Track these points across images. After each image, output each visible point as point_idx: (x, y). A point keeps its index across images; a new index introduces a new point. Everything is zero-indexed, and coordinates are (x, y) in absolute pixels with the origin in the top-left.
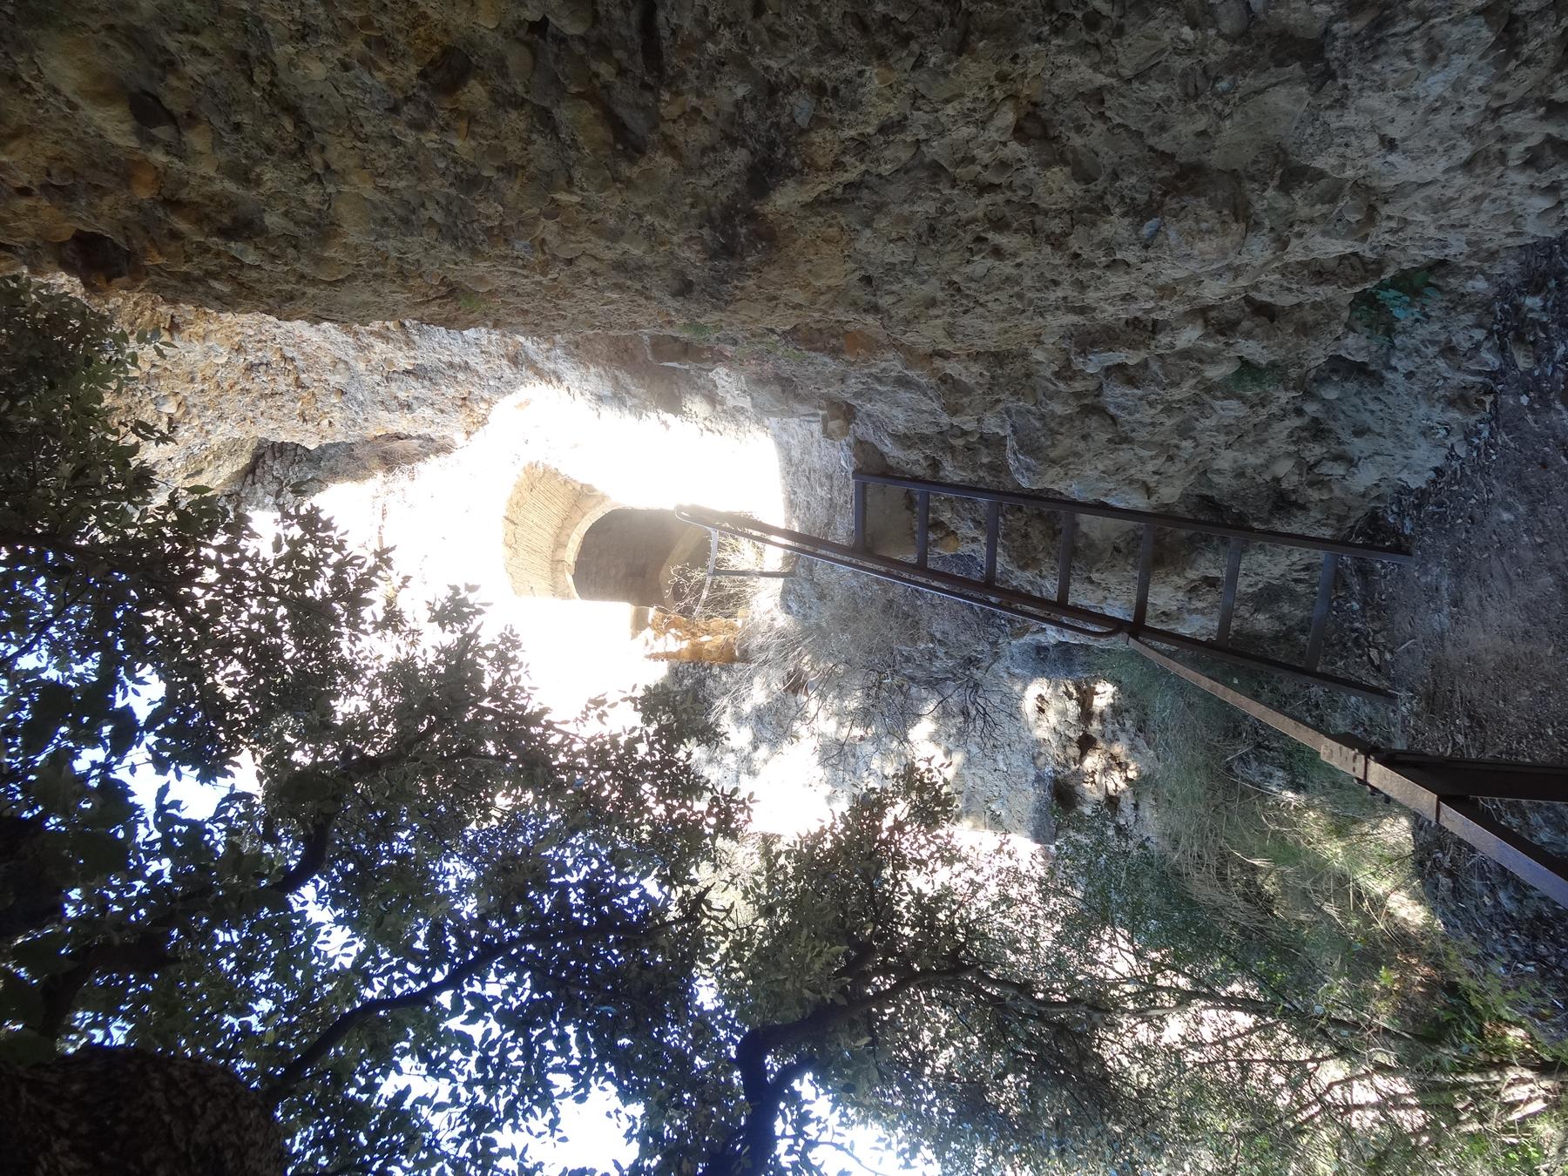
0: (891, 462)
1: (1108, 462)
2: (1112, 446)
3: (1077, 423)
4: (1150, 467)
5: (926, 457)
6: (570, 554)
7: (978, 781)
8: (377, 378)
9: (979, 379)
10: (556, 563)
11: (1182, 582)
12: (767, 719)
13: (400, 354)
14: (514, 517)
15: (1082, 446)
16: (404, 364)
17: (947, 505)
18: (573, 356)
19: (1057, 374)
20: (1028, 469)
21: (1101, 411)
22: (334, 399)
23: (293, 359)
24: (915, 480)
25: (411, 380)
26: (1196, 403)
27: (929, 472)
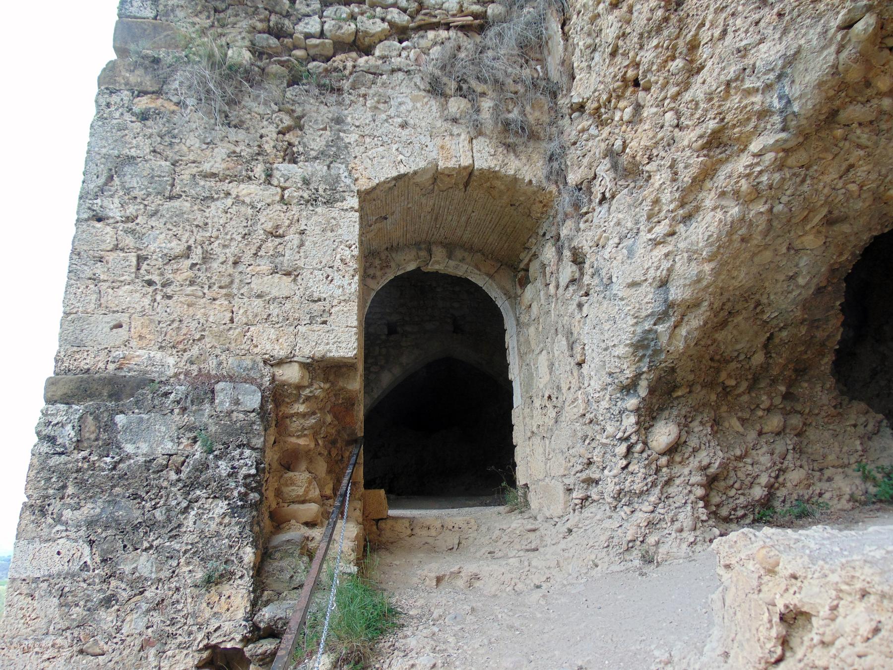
12: (157, 618)
14: (474, 184)
18: (730, 234)
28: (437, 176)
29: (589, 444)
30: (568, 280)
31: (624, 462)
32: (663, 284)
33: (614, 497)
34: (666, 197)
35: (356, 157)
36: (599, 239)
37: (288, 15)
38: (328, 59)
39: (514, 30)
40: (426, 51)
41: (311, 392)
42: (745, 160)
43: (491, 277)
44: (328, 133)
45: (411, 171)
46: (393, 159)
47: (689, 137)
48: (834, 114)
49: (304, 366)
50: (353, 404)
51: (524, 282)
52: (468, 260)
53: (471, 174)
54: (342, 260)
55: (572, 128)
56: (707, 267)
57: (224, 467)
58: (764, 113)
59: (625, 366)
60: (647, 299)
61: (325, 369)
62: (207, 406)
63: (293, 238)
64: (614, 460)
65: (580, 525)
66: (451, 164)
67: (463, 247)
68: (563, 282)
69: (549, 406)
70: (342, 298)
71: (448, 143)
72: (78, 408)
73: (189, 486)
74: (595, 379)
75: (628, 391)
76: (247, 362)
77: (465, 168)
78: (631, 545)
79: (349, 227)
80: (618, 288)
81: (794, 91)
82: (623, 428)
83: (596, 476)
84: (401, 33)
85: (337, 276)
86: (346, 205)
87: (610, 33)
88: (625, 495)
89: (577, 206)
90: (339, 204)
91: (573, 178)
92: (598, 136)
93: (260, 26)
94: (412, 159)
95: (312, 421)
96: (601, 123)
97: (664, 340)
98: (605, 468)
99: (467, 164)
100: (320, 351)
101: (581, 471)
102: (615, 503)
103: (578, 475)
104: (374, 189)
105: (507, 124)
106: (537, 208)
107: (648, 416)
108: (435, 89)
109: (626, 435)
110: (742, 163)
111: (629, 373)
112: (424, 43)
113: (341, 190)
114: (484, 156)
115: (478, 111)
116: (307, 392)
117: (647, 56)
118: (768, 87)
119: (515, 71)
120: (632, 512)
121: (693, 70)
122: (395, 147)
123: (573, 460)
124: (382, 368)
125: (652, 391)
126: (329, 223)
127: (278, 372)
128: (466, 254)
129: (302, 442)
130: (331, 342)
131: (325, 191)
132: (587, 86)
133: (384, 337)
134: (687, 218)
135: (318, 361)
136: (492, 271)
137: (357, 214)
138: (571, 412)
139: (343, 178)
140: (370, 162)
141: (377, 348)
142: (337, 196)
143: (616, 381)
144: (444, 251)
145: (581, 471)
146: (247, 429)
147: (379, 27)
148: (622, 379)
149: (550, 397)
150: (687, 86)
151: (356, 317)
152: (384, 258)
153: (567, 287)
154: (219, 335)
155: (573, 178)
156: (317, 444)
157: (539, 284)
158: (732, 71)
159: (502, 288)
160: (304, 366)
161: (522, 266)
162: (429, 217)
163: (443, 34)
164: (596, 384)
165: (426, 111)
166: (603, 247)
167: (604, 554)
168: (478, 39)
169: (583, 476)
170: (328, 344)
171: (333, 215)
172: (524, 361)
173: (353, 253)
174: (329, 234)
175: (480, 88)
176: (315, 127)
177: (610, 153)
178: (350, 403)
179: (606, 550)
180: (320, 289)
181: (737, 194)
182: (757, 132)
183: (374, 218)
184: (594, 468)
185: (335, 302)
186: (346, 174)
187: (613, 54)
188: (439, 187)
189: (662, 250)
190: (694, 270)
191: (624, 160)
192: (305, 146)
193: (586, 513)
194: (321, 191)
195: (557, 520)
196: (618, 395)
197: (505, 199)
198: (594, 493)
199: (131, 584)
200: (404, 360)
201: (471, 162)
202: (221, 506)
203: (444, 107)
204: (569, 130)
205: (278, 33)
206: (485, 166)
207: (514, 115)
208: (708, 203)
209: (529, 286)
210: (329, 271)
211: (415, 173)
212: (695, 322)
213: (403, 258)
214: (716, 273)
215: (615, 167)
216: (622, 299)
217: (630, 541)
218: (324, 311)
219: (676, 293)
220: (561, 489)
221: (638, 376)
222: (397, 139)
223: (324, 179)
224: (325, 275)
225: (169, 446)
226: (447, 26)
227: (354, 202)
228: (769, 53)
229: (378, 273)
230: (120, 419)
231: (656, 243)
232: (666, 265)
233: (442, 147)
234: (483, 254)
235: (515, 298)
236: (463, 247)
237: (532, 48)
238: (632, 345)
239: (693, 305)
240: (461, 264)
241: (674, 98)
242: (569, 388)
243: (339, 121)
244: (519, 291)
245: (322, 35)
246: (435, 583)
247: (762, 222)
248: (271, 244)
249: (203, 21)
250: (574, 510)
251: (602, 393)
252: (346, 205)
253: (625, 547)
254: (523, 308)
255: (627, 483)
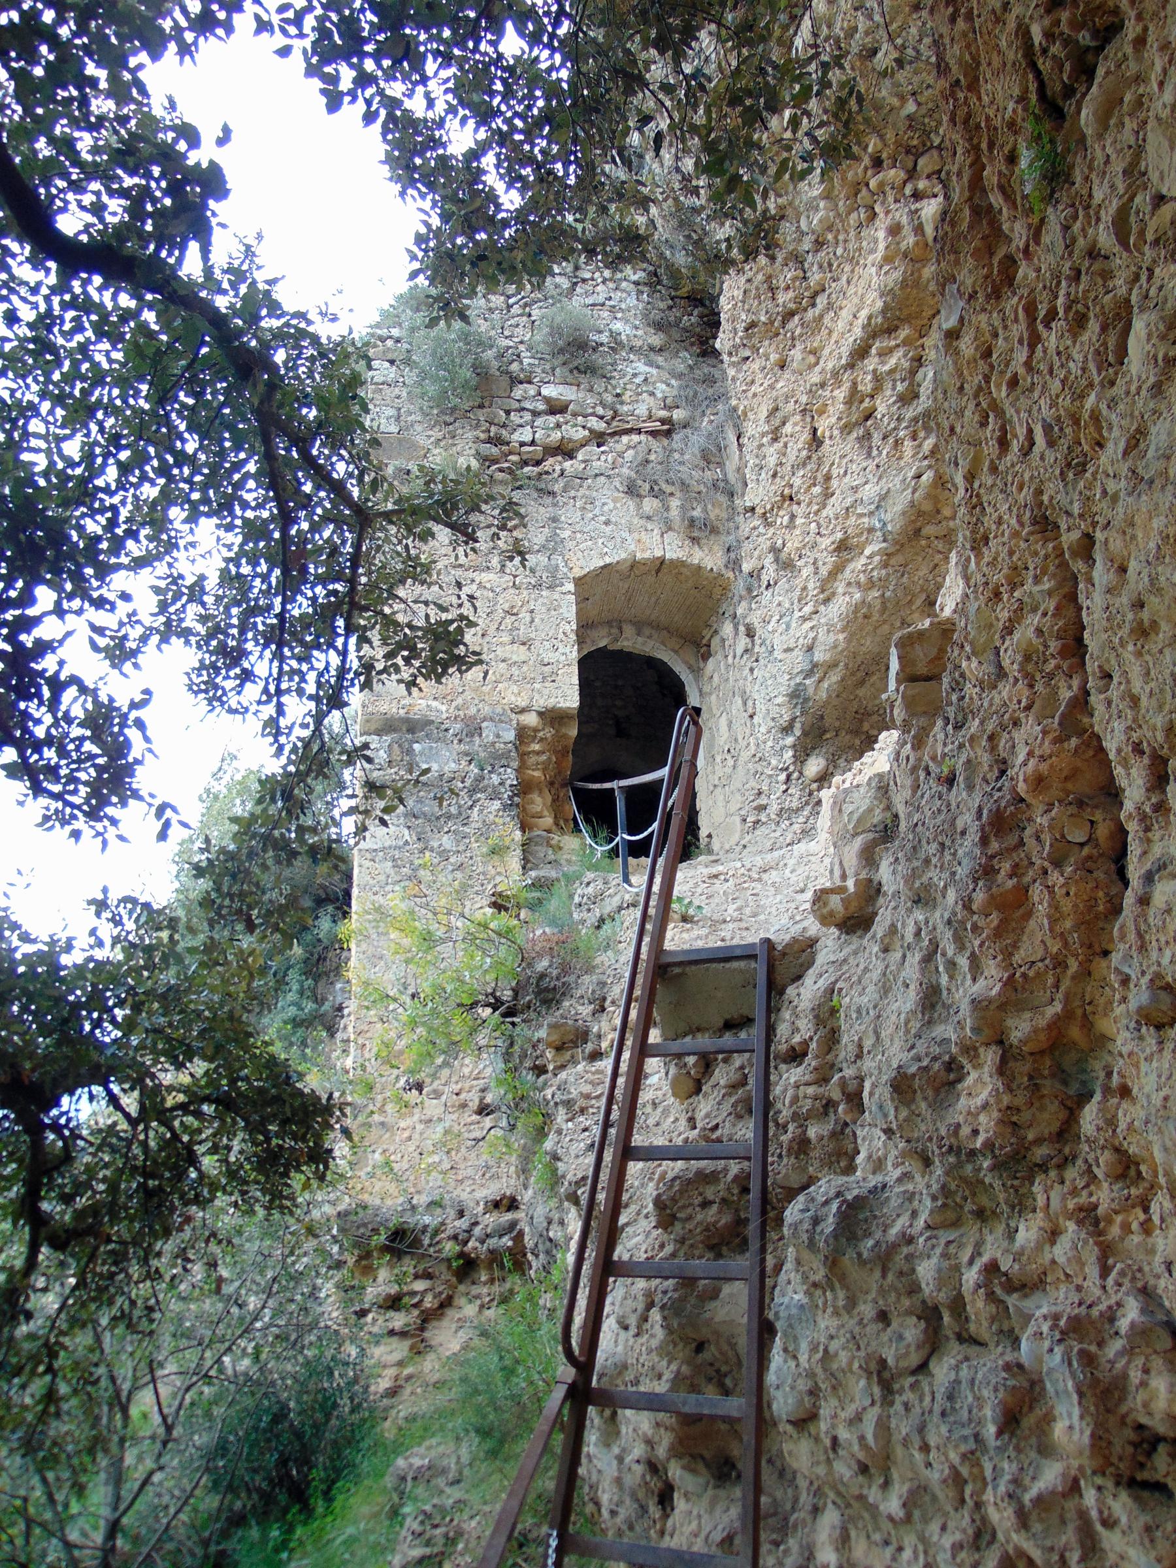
0: (791, 991)
1: (843, 1357)
2: (873, 1366)
3: (906, 1302)
4: (844, 1434)
5: (805, 1043)
6: (631, 642)
7: (406, 1134)
8: (804, 399)
9: (965, 1131)
10: (616, 624)
11: (661, 1452)
12: (459, 875)
13: (833, 420)
14: (664, 570)
15: (867, 1310)
16: (824, 425)
17: (738, 1076)
18: (855, 612)
19: (992, 1268)
20: (816, 1221)
21: (933, 1344)
22: (774, 357)
23: (814, 305)
24: (770, 1030)
25: (806, 436)
26: (978, 1535)
27: (783, 1048)
28: (634, 564)
32: (810, 649)
34: (811, 586)
37: (504, 426)
38: (538, 463)
39: (697, 440)
40: (621, 455)
42: (863, 560)
47: (825, 542)
48: (918, 531)
49: (540, 714)
51: (706, 656)
55: (746, 525)
56: (841, 637)
57: (495, 779)
58: (871, 530)
60: (798, 660)
61: (553, 717)
62: (477, 739)
63: (525, 616)
66: (647, 555)
67: (650, 624)
68: (739, 651)
72: (387, 739)
73: (472, 791)
74: (762, 724)
76: (499, 710)
79: (569, 610)
81: (889, 517)
84: (599, 438)
87: (772, 461)
89: (749, 590)
91: (746, 567)
93: (483, 436)
95: (544, 758)
96: (768, 525)
97: (811, 691)
100: (551, 703)
105: (692, 522)
106: (718, 591)
107: (803, 753)
108: (631, 490)
110: (859, 563)
111: (786, 717)
112: (619, 447)
114: (673, 548)
115: (667, 509)
117: (797, 481)
118: (871, 513)
119: (696, 474)
121: (827, 494)
125: (805, 734)
127: (522, 718)
129: (537, 774)
132: (758, 493)
134: (826, 601)
138: (745, 755)
146: (506, 755)
147: (580, 434)
150: (824, 506)
154: (476, 690)
155: (746, 567)
157: (719, 657)
158: (848, 501)
159: (686, 662)
160: (540, 714)
163: (635, 438)
164: (763, 729)
165: (625, 510)
168: (666, 442)
175: (668, 489)
177: (775, 550)
180: (550, 656)
181: (858, 584)
182: (868, 542)
187: (774, 476)
189: (808, 624)
190: (832, 638)
191: (783, 556)
197: (690, 584)
199: (440, 854)
202: (497, 804)
203: (639, 507)
205: (497, 441)
207: (697, 513)
208: (840, 590)
212: (834, 678)
214: (848, 640)
215: (777, 560)
219: (819, 656)
221: (793, 720)
223: (546, 569)
225: (453, 766)
226: (639, 431)
227: (571, 587)
228: (870, 491)
230: (416, 746)
231: (805, 619)
232: (811, 635)
236: (650, 624)
237: (711, 457)
239: (833, 665)
241: (816, 513)
243: (555, 520)
245: (533, 443)
247: (877, 604)
248: (509, 620)
249: (436, 434)
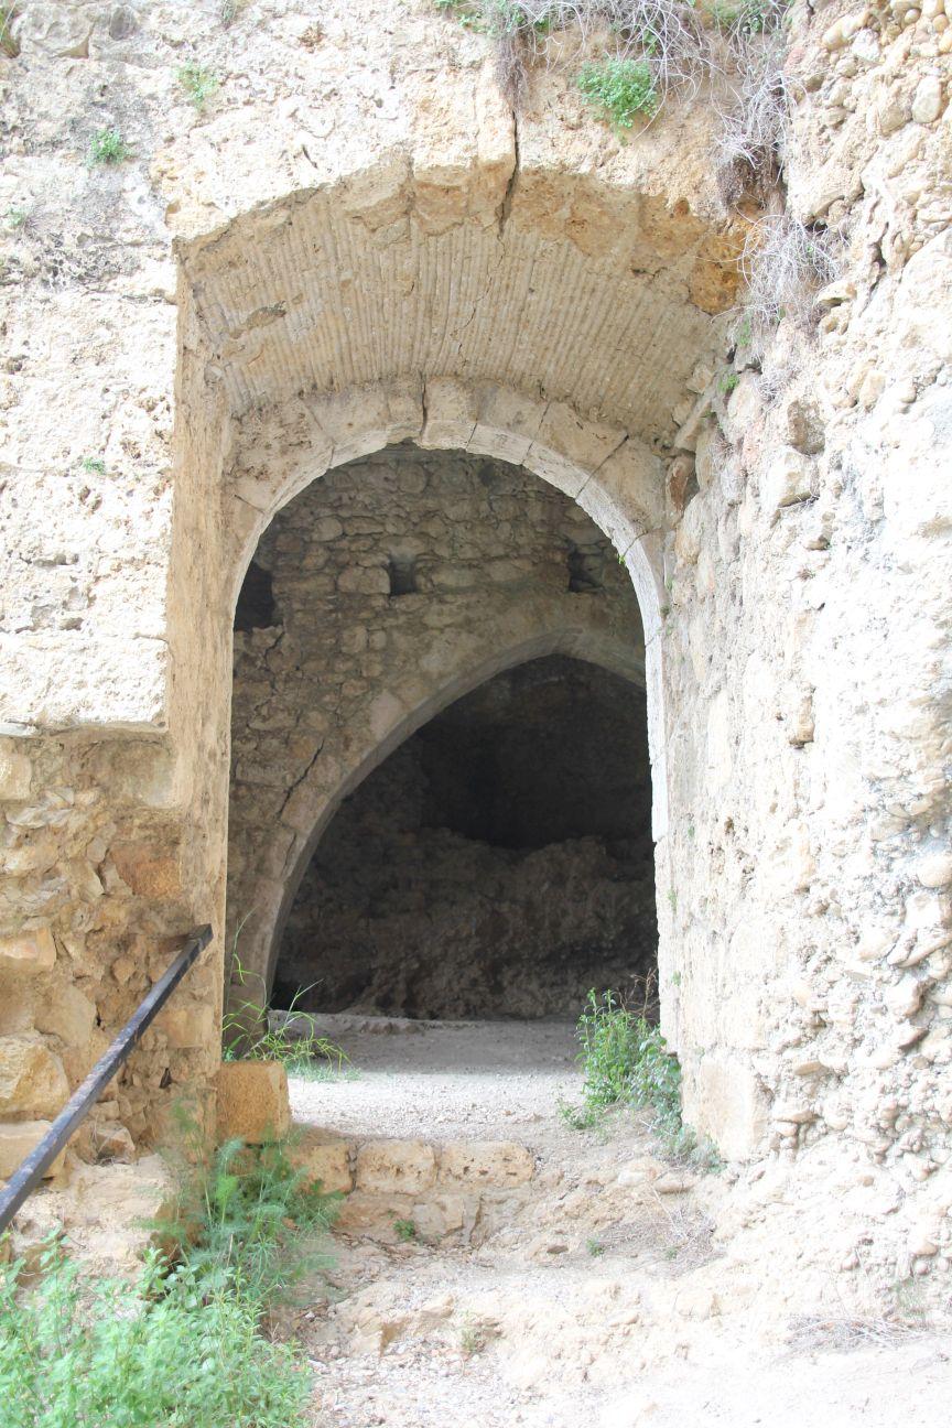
29: (818, 971)
30: (778, 500)
31: (908, 1032)
33: (878, 1128)
35: (171, 140)
36: (859, 385)
41: (38, 817)
43: (596, 471)
44: (92, 66)
45: (332, 180)
46: (278, 146)
50: (176, 843)
51: (686, 489)
52: (533, 423)
53: (511, 184)
54: (125, 445)
59: (911, 764)
61: (101, 754)
64: (880, 1020)
65: (787, 1198)
66: (449, 156)
69: (729, 850)
70: (125, 555)
71: (443, 91)
74: (844, 796)
75: (925, 831)
77: (493, 168)
78: (920, 1266)
79: (149, 347)
80: (898, 537)
82: (906, 935)
83: (834, 1062)
85: (106, 489)
86: (141, 283)
88: (911, 1123)
90: (121, 280)
92: (875, 64)
94: (336, 141)
98: (857, 1042)
99: (494, 157)
100: (58, 706)
101: (798, 1044)
102: (880, 1145)
103: (789, 1053)
104: (224, 234)
109: (917, 954)
113: (128, 238)
116: (26, 817)
120: (930, 1172)
122: (286, 107)
123: (779, 1012)
124: (373, 685)
126: (92, 337)
128: (527, 407)
130: (91, 680)
131: (81, 240)
133: (379, 602)
135: (54, 733)
136: (599, 456)
137: (173, 311)
139: (134, 205)
140: (212, 153)
141: (360, 632)
142: (117, 257)
143: (889, 802)
144: (464, 396)
145: (798, 1044)
148: (905, 797)
149: (730, 825)
151: (161, 609)
152: (291, 418)
153: (778, 517)
156: (62, 955)
159: (626, 503)
161: (681, 441)
162: (406, 307)
166: (868, 409)
167: (842, 1287)
169: (801, 1057)
170: (81, 685)
171: (103, 313)
172: (678, 713)
173: (159, 426)
174: (90, 369)
176: (54, 44)
178: (168, 837)
179: (848, 1275)
180: (76, 532)
183: (244, 316)
184: (830, 1037)
185: (104, 569)
186: (144, 190)
188: (422, 222)
192: (24, 106)
193: (809, 1158)
194: (69, 242)
195: (739, 1169)
196: (896, 841)
198: (830, 1103)
200: (432, 663)
201: (508, 148)
204: (799, 43)
206: (549, 159)
209: (694, 502)
210: (90, 480)
211: (344, 185)
213: (346, 419)
216: (907, 569)
217: (916, 1258)
218: (73, 591)
220: (747, 1087)
222: (292, 82)
224: (78, 490)
227: (164, 274)
229: (276, 465)
233: (425, 106)
234: (574, 407)
235: (662, 533)
236: (517, 385)
238: (931, 703)
240: (512, 436)
242: (773, 809)
244: (673, 515)
246: (376, 1344)
250: (777, 1149)
251: (853, 833)
252: (141, 283)
253: (902, 1271)
254: (680, 562)
255: (916, 1092)
